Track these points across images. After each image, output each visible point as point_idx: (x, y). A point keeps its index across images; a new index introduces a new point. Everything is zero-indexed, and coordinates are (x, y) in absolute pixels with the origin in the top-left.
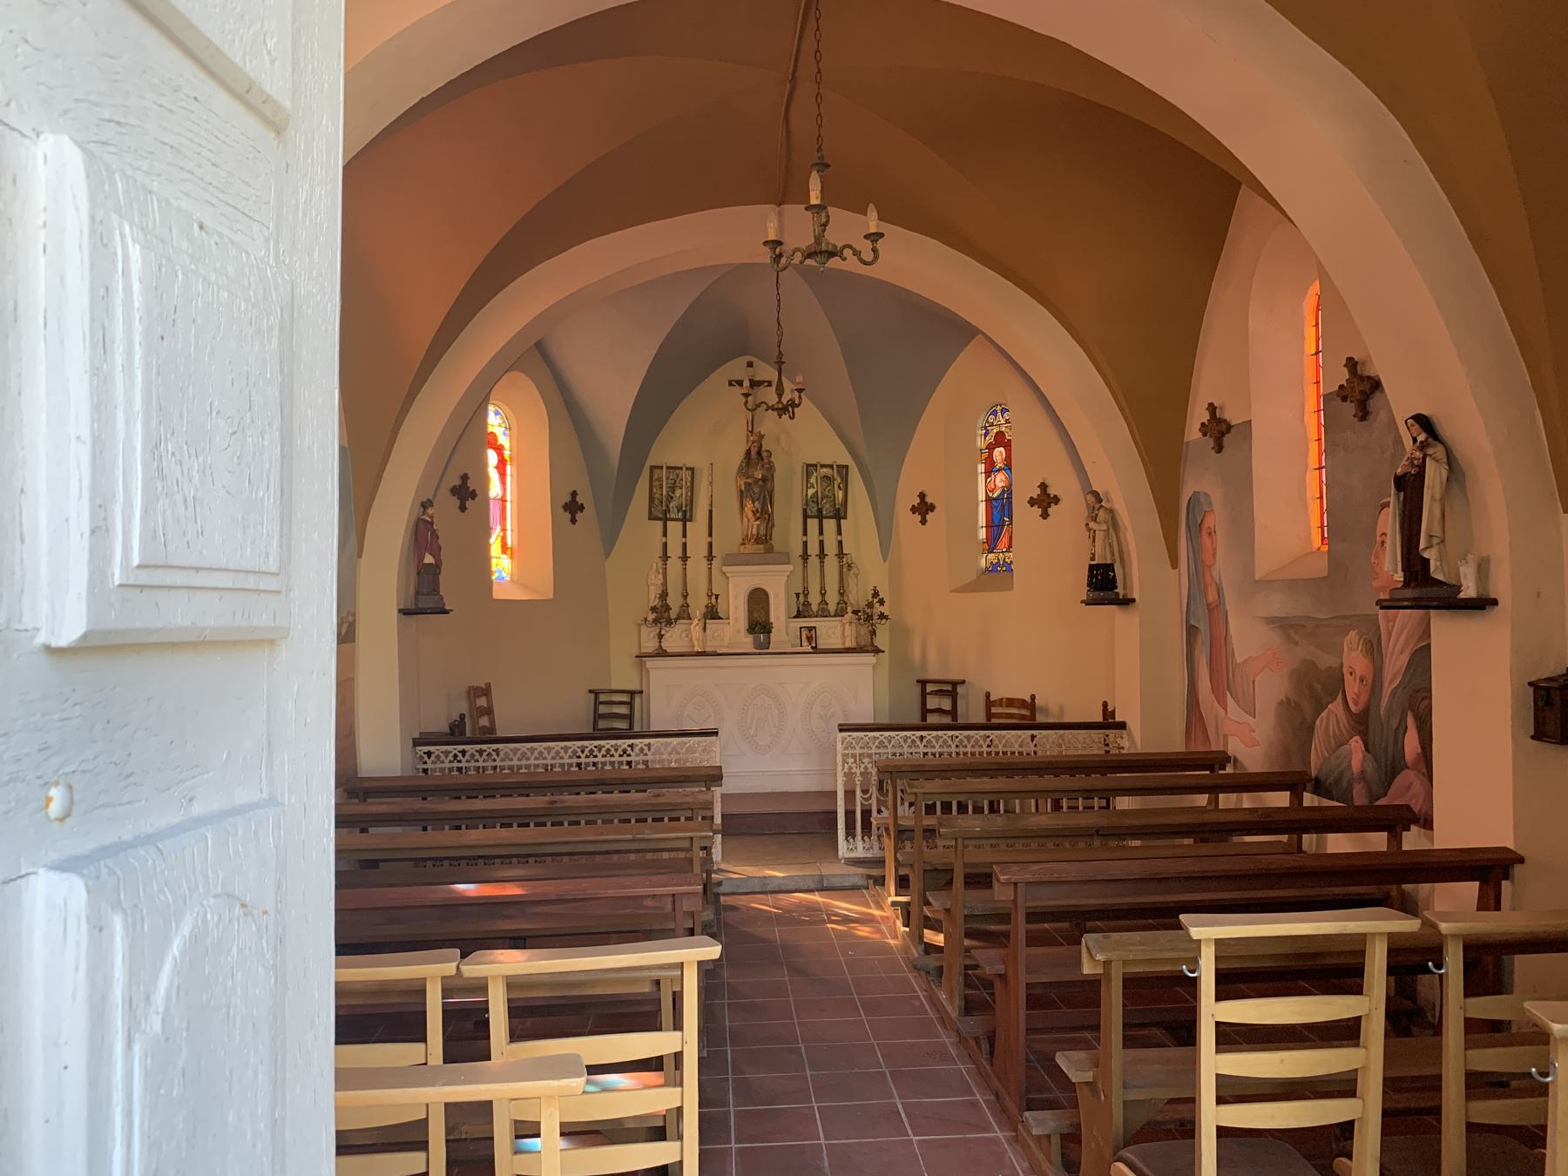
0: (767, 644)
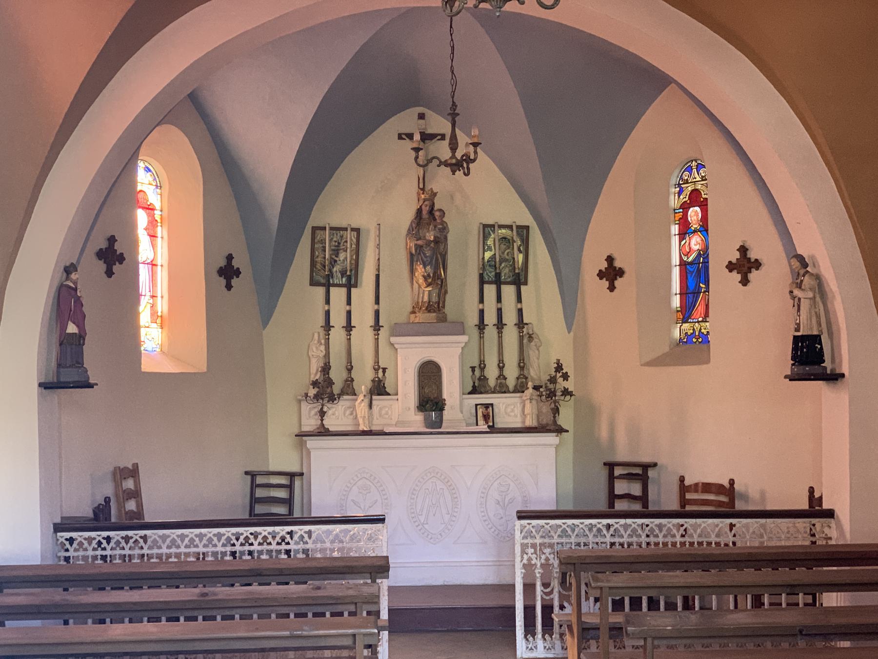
0: (439, 423)
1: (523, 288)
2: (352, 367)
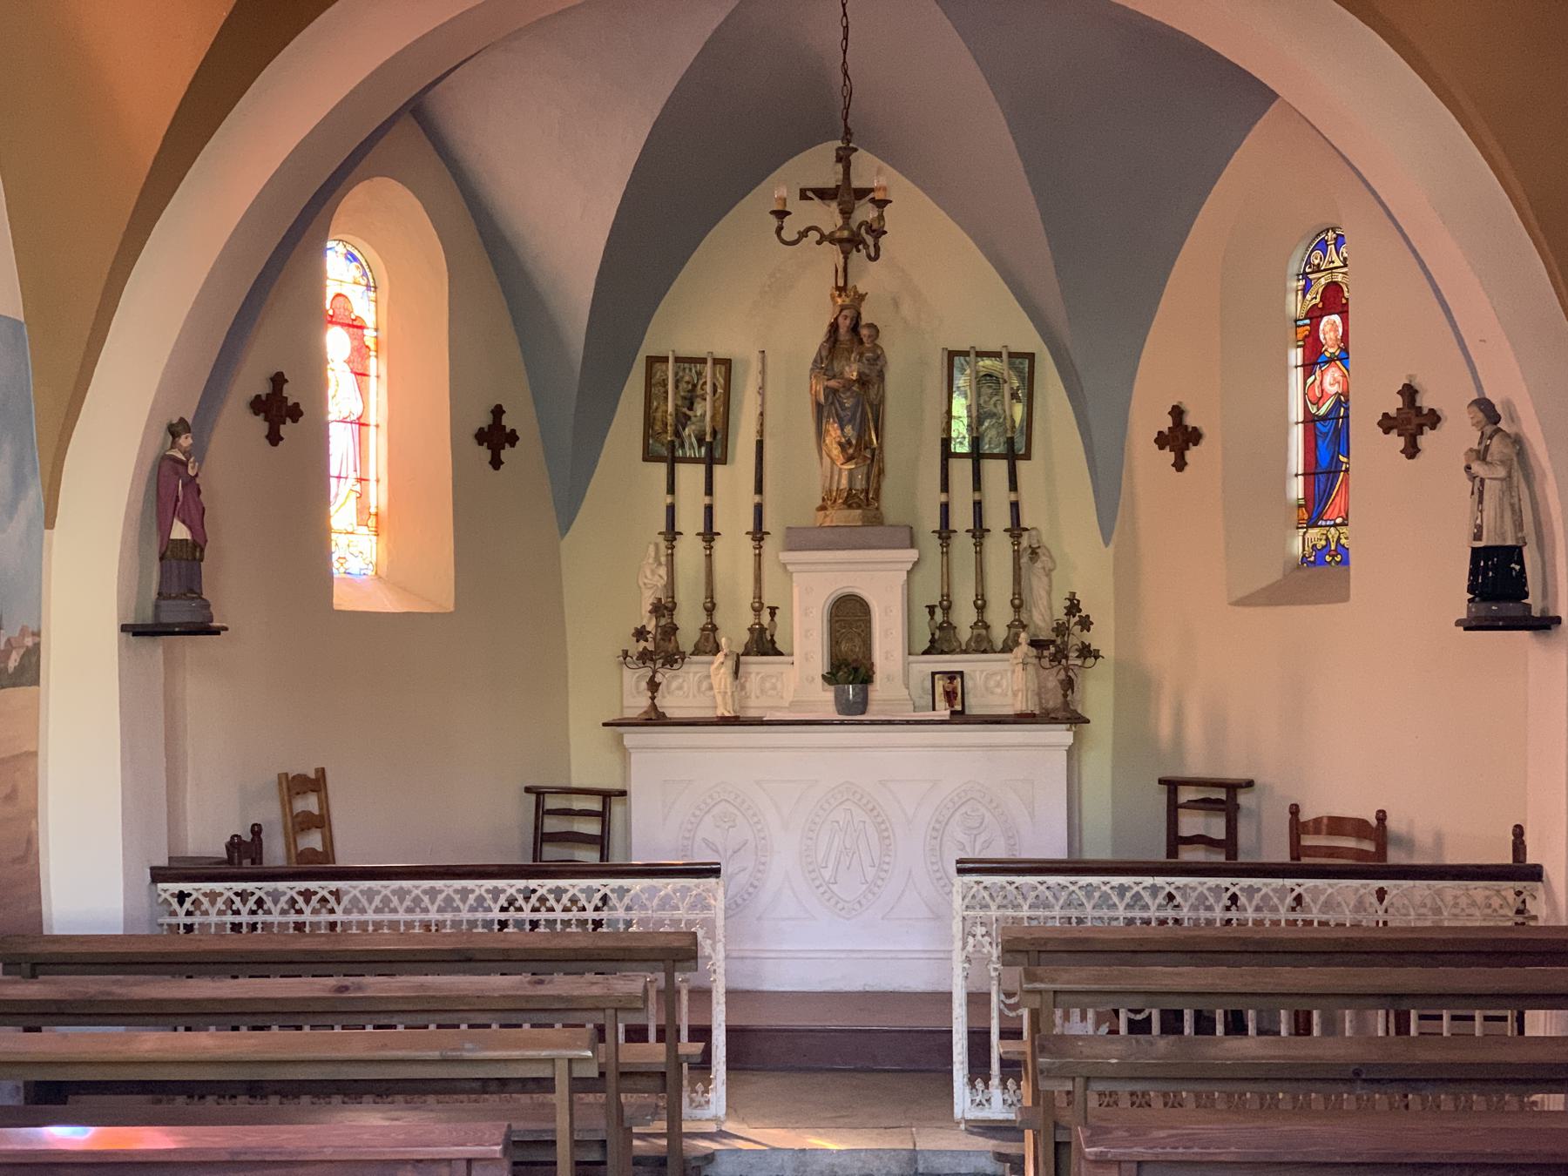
0: (862, 704)
1: (1022, 466)
2: (714, 605)
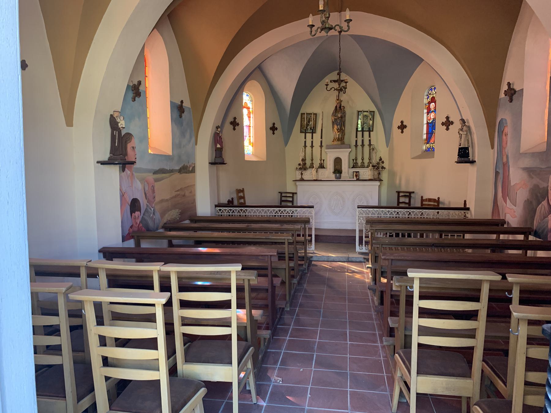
0: (340, 177)
1: (371, 133)
